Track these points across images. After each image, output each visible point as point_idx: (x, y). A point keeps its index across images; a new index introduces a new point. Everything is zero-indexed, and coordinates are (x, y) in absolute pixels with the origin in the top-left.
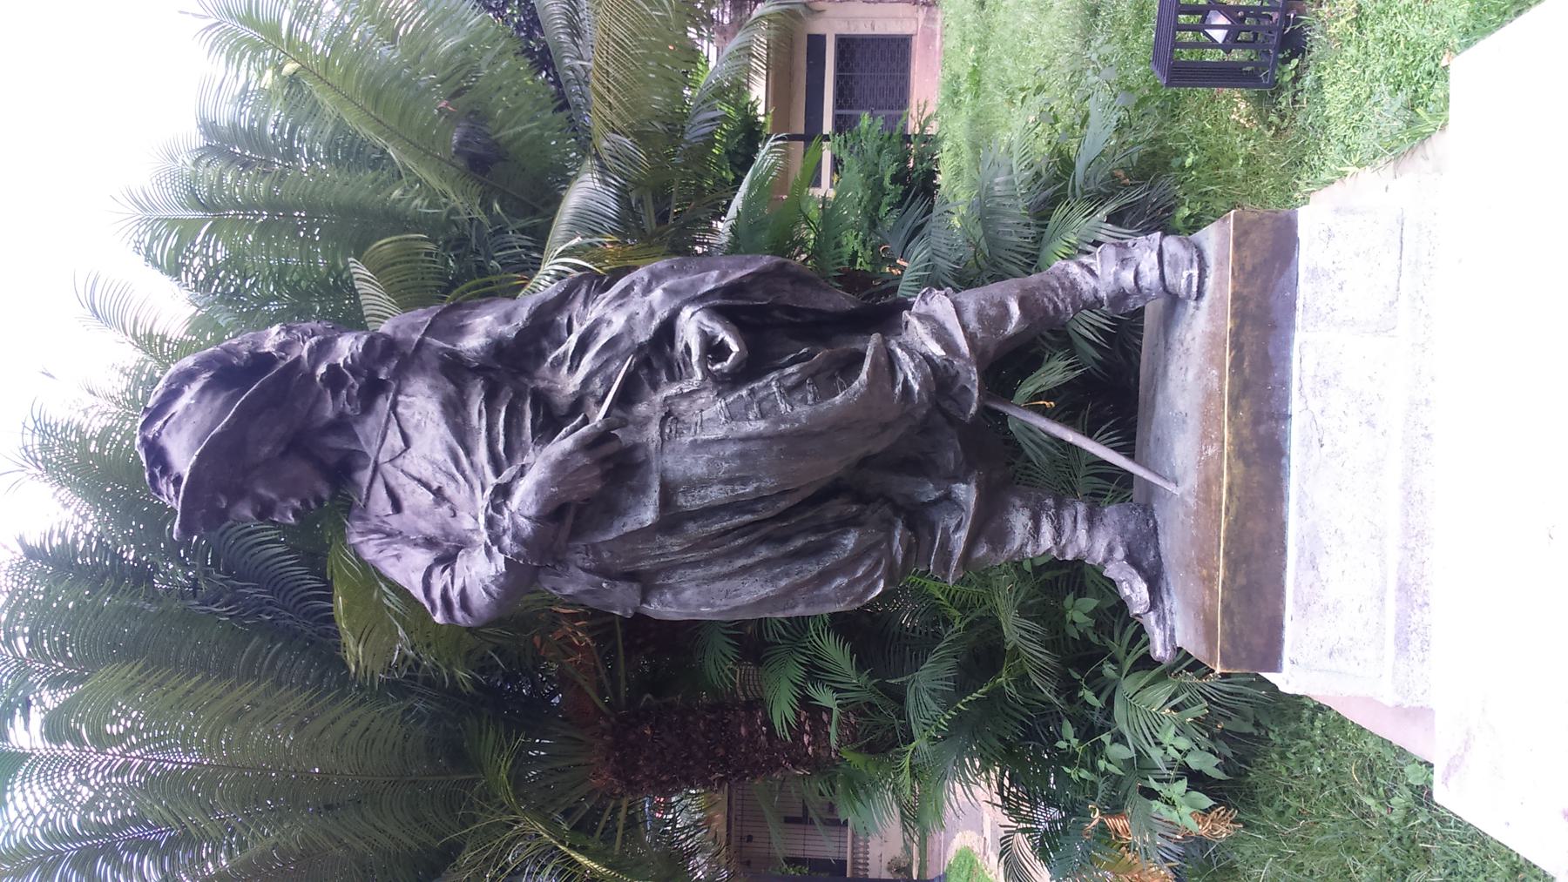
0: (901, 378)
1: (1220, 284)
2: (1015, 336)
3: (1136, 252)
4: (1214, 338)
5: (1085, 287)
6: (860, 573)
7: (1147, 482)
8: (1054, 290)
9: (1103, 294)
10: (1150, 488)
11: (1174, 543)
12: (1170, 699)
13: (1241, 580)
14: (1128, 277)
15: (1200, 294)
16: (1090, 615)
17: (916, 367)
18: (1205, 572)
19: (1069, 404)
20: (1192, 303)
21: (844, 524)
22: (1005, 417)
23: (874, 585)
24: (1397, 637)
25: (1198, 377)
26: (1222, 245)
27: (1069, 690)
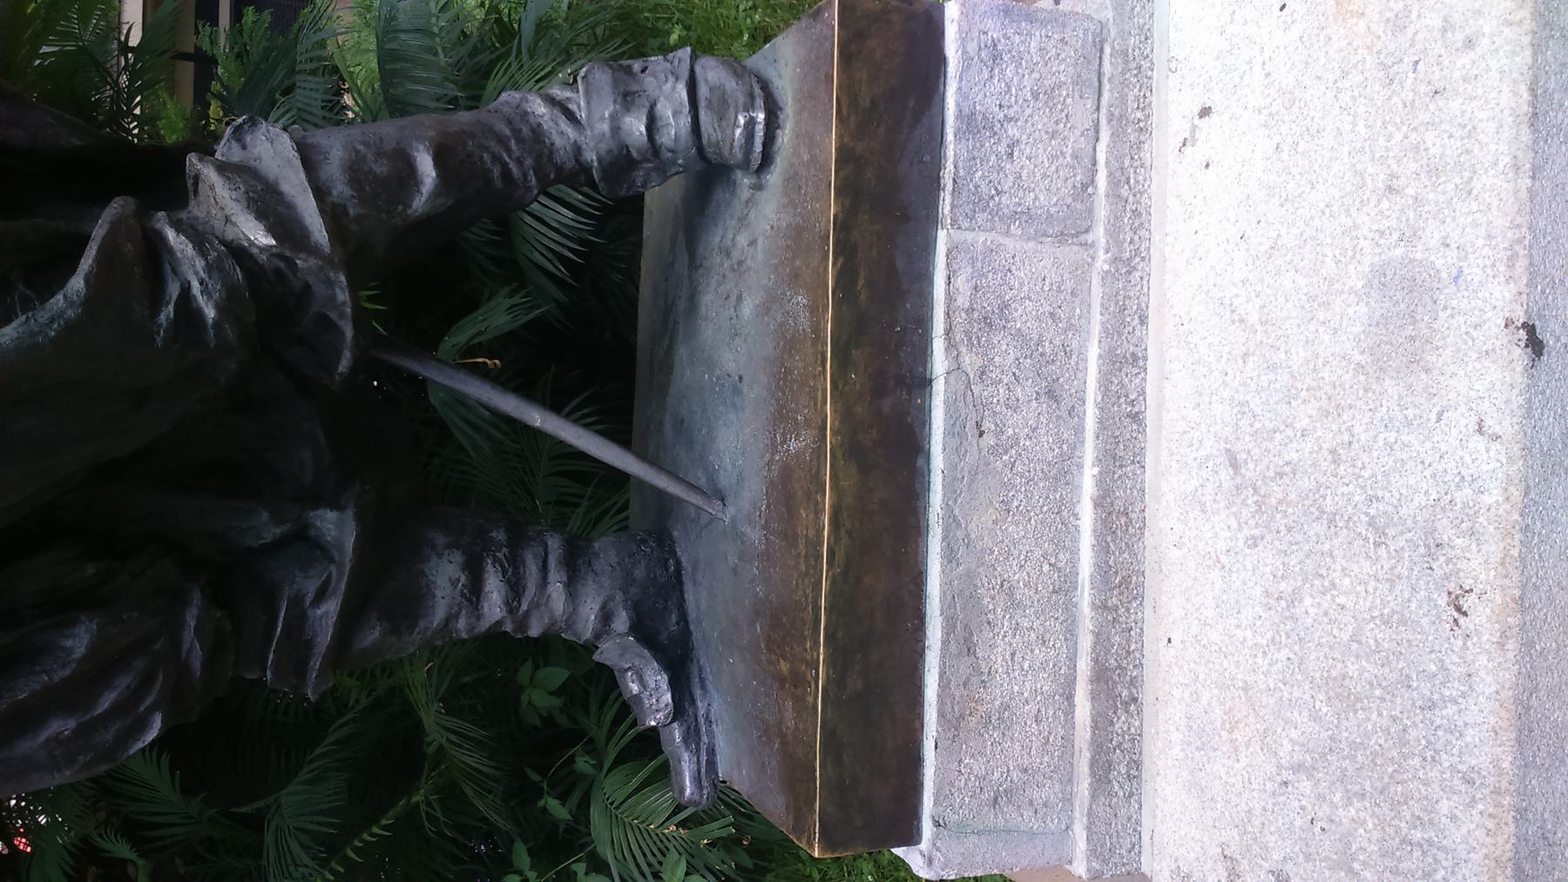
0: (174, 290)
1: (806, 138)
2: (428, 221)
3: (649, 82)
4: (797, 238)
5: (559, 142)
6: (106, 702)
7: (660, 493)
8: (502, 140)
9: (591, 156)
10: (664, 506)
11: (717, 598)
12: (674, 813)
13: (855, 683)
14: (636, 126)
15: (767, 158)
16: (560, 692)
17: (209, 268)
18: (784, 667)
19: (529, 363)
20: (745, 181)
21: (64, 606)
22: (420, 384)
23: (141, 725)
24: (1093, 763)
25: (765, 310)
26: (813, 68)
27: (522, 795)
